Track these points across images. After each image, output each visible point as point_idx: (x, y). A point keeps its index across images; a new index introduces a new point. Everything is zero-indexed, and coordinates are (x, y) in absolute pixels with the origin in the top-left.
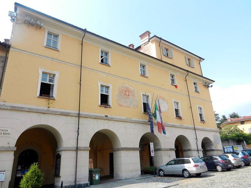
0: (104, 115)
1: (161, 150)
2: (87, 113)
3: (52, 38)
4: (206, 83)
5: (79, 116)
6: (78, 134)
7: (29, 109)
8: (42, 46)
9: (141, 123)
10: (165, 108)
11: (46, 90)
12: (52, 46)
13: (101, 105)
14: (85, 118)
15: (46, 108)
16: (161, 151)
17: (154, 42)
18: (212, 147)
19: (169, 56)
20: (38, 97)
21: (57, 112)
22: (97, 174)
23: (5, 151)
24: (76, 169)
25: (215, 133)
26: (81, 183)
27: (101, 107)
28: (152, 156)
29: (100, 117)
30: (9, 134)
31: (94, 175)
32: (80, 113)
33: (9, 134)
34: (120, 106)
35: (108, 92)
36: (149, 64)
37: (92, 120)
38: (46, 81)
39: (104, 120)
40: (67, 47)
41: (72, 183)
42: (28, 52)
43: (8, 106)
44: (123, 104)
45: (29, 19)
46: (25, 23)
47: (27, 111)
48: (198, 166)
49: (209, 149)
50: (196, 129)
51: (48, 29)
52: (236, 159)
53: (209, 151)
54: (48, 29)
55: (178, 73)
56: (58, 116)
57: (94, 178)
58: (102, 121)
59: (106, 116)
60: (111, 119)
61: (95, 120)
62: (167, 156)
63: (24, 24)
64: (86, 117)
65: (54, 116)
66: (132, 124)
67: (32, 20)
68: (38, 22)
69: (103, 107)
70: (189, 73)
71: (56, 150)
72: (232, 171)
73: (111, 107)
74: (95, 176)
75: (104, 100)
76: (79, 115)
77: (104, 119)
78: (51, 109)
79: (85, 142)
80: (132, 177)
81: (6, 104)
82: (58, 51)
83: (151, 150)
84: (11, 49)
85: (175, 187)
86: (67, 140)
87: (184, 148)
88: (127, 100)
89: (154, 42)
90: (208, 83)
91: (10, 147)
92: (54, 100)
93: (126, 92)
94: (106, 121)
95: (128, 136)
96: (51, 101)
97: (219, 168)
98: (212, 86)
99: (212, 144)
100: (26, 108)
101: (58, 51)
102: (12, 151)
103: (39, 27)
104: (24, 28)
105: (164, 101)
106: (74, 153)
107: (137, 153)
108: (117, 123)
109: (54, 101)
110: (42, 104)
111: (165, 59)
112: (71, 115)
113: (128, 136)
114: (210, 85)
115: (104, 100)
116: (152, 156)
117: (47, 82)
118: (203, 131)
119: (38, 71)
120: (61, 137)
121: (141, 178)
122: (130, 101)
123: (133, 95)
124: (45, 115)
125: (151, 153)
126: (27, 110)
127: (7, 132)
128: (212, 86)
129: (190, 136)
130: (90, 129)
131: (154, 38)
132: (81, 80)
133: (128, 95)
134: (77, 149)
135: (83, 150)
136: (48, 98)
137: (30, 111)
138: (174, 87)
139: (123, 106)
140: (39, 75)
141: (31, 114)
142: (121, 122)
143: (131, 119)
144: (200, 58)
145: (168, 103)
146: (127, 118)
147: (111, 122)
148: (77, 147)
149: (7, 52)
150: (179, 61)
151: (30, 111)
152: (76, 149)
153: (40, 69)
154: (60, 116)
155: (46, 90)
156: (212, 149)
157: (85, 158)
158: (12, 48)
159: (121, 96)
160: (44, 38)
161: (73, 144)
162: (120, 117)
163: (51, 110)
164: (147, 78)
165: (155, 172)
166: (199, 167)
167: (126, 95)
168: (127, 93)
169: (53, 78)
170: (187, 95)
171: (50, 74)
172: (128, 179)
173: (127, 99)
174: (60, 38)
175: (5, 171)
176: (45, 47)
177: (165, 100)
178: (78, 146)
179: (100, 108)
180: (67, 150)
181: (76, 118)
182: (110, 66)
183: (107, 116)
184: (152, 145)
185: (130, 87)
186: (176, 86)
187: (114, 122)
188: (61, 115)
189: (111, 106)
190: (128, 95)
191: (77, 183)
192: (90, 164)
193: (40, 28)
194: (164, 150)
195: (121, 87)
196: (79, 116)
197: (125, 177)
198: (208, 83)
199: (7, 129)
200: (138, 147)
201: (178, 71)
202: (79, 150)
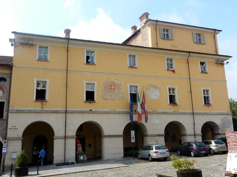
1: (148, 136)
2: (73, 109)
3: (43, 50)
4: (218, 61)
5: (66, 112)
7: (29, 110)
8: (84, 64)
9: (126, 113)
10: (156, 96)
11: (41, 95)
12: (43, 59)
13: (205, 104)
14: (72, 114)
15: (41, 109)
16: (148, 137)
17: (150, 26)
18: (219, 131)
19: (201, 43)
20: (35, 101)
21: (48, 111)
22: (82, 155)
23: (16, 140)
24: (65, 151)
25: (224, 116)
26: (69, 162)
27: (86, 103)
28: (132, 142)
29: (184, 113)
30: (17, 129)
31: (79, 157)
33: (17, 129)
34: (105, 99)
35: (93, 89)
36: (141, 54)
37: (77, 115)
38: (171, 94)
39: (88, 114)
41: (63, 161)
42: (25, 68)
43: (15, 110)
44: (108, 98)
45: (23, 41)
46: (21, 44)
47: (28, 113)
48: (158, 152)
49: (216, 132)
50: (67, 112)
51: (39, 44)
52: (217, 146)
53: (216, 135)
54: (39, 44)
55: (178, 55)
56: (50, 114)
57: (79, 159)
58: (87, 114)
59: (90, 110)
60: (96, 112)
61: (80, 114)
62: (154, 141)
63: (20, 46)
64: (73, 112)
65: (47, 114)
66: (116, 114)
67: (26, 41)
68: (30, 42)
69: (88, 102)
70: (191, 54)
71: (53, 137)
72: (209, 156)
74: (80, 157)
75: (90, 96)
76: (66, 112)
77: (89, 113)
78: (45, 109)
79: (72, 131)
80: (115, 159)
81: (14, 109)
82: (48, 61)
83: (132, 137)
84: (13, 68)
85: (73, 175)
86: (58, 131)
87: (182, 133)
88: (113, 93)
89: (150, 26)
90: (221, 61)
91: (18, 137)
92: (47, 101)
93: (111, 86)
94: (90, 114)
95: (113, 125)
96: (44, 103)
97: (192, 154)
98: (227, 63)
99: (219, 128)
100: (26, 110)
101: (48, 61)
102: (20, 140)
103: (32, 45)
104: (21, 48)
105: (156, 89)
106: (63, 141)
107: (121, 140)
108: (101, 115)
109: (46, 102)
110: (38, 106)
111: (164, 44)
112: (60, 112)
113: (113, 125)
114: (225, 62)
115: (90, 96)
116: (132, 142)
117: (90, 90)
118: (205, 115)
119: (34, 81)
120: (102, 129)
121: (123, 159)
122: (116, 94)
123: (120, 88)
124: (40, 114)
125: (132, 140)
126: (204, 114)
127: (16, 128)
128: (227, 63)
129: (186, 122)
130: (201, 121)
131: (149, 22)
132: (67, 83)
133: (114, 89)
134: (65, 138)
135: (70, 138)
136: (42, 101)
137: (30, 112)
138: (172, 72)
139: (108, 100)
140: (34, 84)
141: (30, 114)
142: (105, 114)
143: (115, 110)
144: (215, 30)
145: (160, 91)
146: (111, 110)
147: (95, 115)
148: (65, 136)
149: (11, 70)
150: (184, 42)
151: (30, 112)
152: (64, 138)
153: (128, 84)
154: (51, 113)
155: (41, 95)
156: (219, 133)
157: (72, 144)
158: (14, 67)
159: (106, 91)
160: (36, 53)
161: (62, 134)
162: (105, 110)
163: (44, 110)
164: (137, 68)
166: (159, 153)
167: (111, 89)
168: (113, 87)
169: (45, 84)
170: (191, 79)
171: (43, 82)
172: (110, 160)
173: (112, 92)
174: (136, 58)
175: (16, 152)
176: (38, 60)
177: (157, 88)
178: (66, 135)
179: (85, 104)
180: (58, 138)
181: (63, 114)
182: (95, 65)
183: (91, 110)
184: (133, 132)
185: (116, 81)
186: (174, 71)
187: (98, 114)
188: (52, 113)
190: (114, 89)
191: (66, 161)
193: (33, 46)
194: (150, 136)
195: (107, 82)
197: (108, 158)
198: (221, 61)
199: (15, 126)
201: (177, 54)
202: (67, 138)
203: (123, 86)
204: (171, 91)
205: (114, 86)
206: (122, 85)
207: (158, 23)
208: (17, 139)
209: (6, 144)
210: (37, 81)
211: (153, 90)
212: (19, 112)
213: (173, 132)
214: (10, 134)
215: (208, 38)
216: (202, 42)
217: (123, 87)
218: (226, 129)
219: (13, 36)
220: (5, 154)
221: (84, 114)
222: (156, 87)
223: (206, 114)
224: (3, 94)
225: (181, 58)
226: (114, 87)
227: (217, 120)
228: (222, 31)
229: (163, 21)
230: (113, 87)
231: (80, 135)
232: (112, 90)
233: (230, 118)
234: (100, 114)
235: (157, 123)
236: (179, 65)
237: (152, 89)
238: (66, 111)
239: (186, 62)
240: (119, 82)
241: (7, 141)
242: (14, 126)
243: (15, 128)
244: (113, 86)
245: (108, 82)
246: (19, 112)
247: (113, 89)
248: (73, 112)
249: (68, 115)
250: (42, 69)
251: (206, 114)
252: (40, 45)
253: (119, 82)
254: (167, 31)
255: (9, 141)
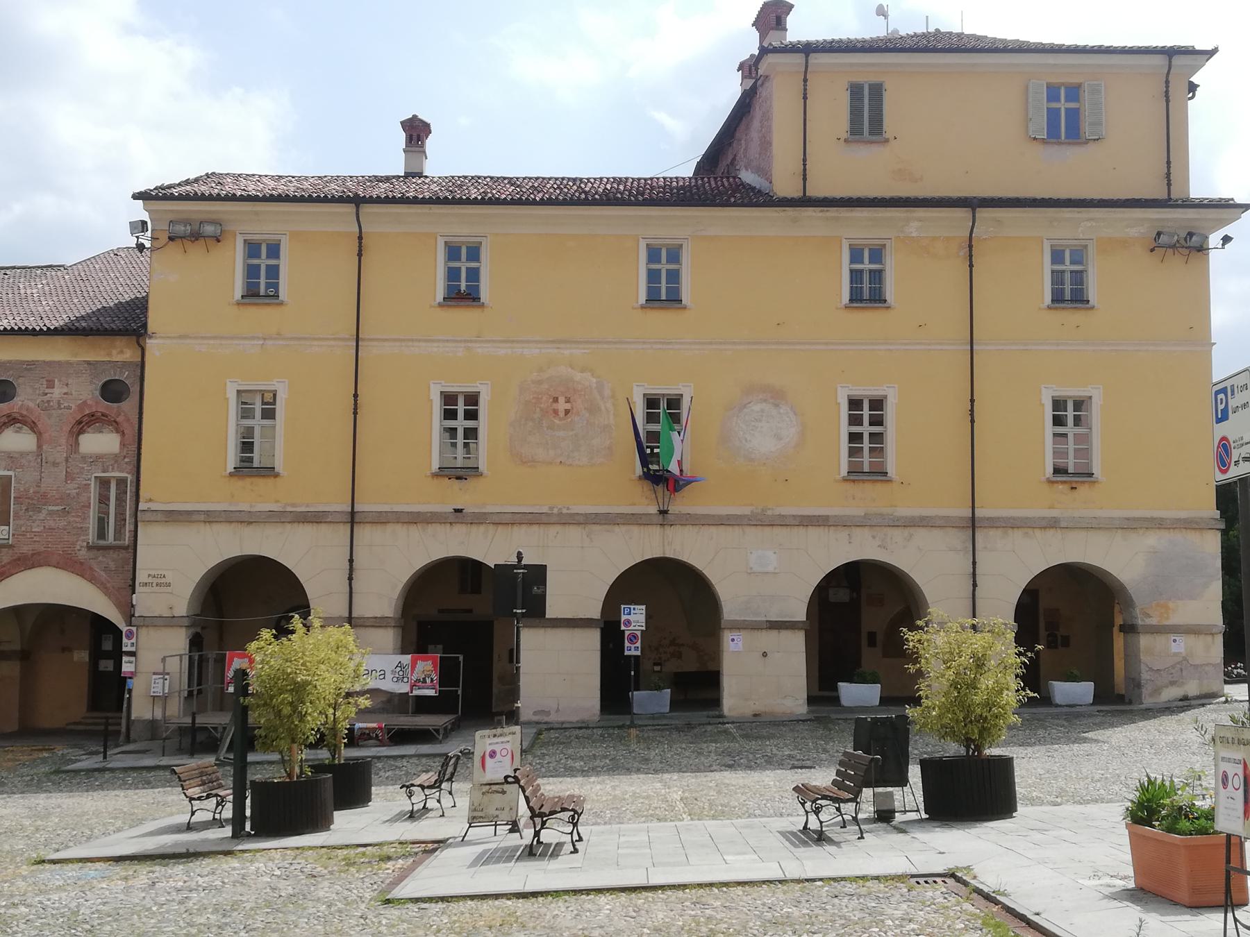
0: (449, 509)
5: (353, 518)
6: (975, 585)
10: (778, 437)
14: (379, 526)
28: (627, 653)
30: (169, 585)
32: (978, 513)
37: (400, 530)
40: (312, 273)
59: (457, 511)
60: (479, 519)
61: (413, 528)
64: (381, 519)
73: (277, 475)
79: (1000, 609)
81: (154, 506)
88: (561, 433)
93: (556, 400)
105: (777, 406)
114: (1214, 239)
116: (627, 653)
123: (593, 409)
124: (251, 527)
125: (627, 644)
127: (163, 580)
128: (1226, 239)
129: (928, 563)
130: (1013, 566)
137: (210, 518)
147: (478, 532)
151: (210, 518)
153: (1044, 390)
165: (403, 711)
167: (556, 412)
168: (562, 406)
171: (263, 393)
181: (341, 526)
185: (578, 376)
189: (485, 472)
192: (711, 667)
196: (353, 518)
200: (801, 616)
203: (613, 397)
204: (866, 413)
205: (568, 401)
206: (607, 392)
207: (816, 59)
208: (169, 622)
209: (134, 640)
210: (239, 392)
211: (762, 411)
212: (173, 517)
213: (859, 618)
214: (146, 602)
215: (1123, 113)
216: (1087, 130)
217: (609, 405)
218: (1171, 605)
219: (139, 211)
220: (132, 675)
221: (431, 529)
222: (776, 396)
223: (1052, 524)
224: (123, 444)
225: (934, 239)
226: (568, 406)
227: (1121, 559)
228: (1214, 52)
229: (1107, 44)
230: (562, 406)
231: (470, 611)
232: (560, 419)
233: (1211, 546)
234: (500, 527)
235: (771, 569)
236: (920, 272)
237: (757, 408)
238: (353, 513)
239: (962, 254)
240: (594, 380)
241: (134, 629)
242: (152, 573)
243: (161, 583)
244: (562, 400)
245: (540, 382)
246: (173, 517)
247: (562, 414)
248: (381, 519)
249: (365, 534)
250: (258, 338)
251: (1052, 524)
252: (249, 237)
253: (594, 380)
254: (1074, 92)
255: (143, 631)
